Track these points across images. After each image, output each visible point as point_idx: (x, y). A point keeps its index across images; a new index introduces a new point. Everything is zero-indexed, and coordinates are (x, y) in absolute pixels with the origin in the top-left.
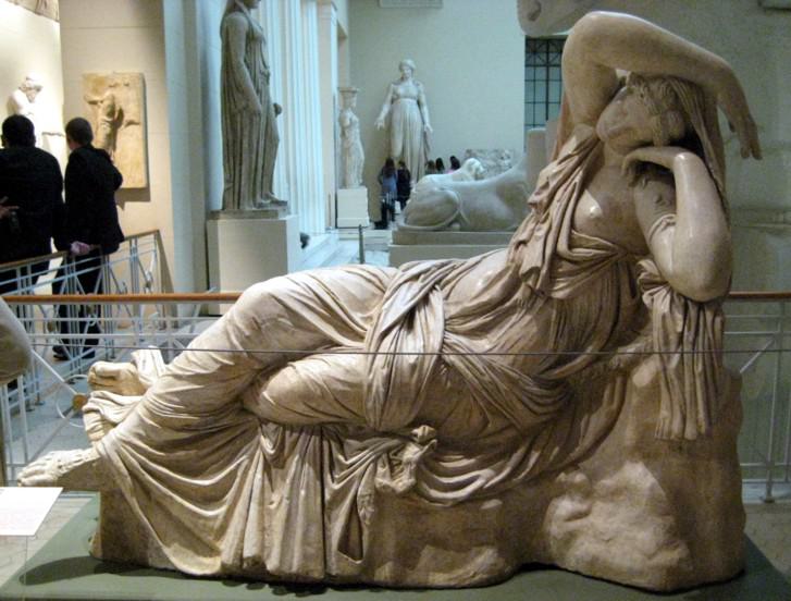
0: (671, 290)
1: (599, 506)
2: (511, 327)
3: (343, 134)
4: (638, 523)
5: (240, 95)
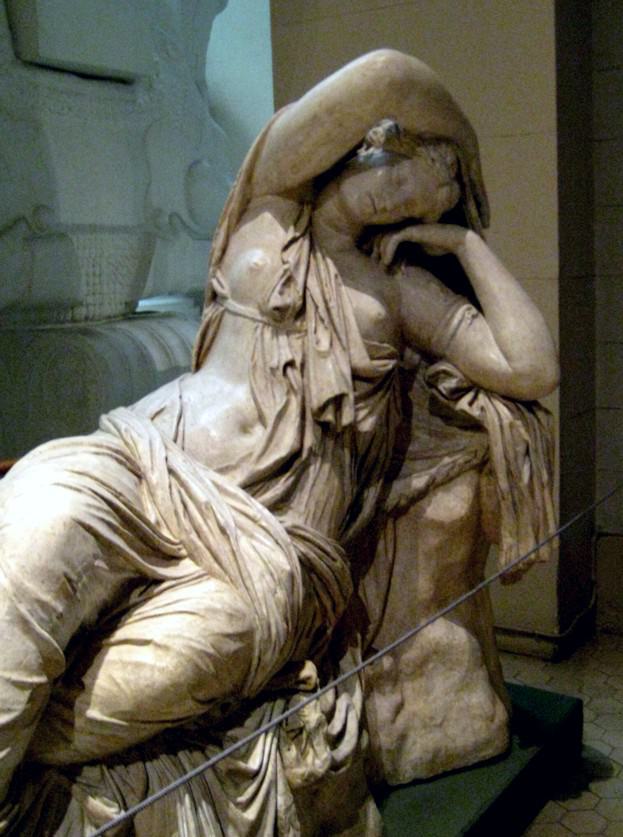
0: (490, 393)
1: (409, 688)
4: (465, 686)
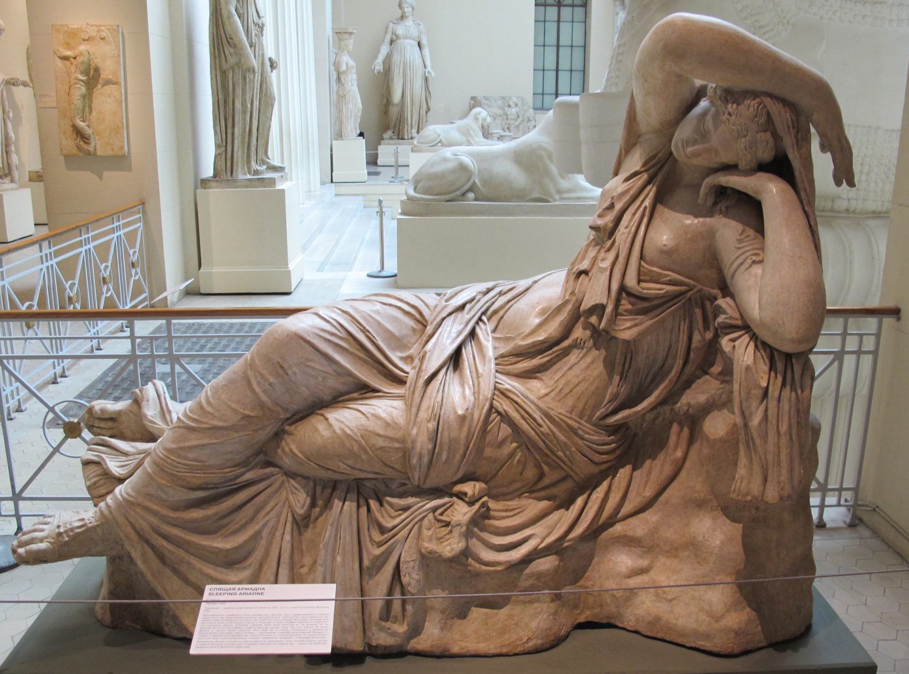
0: (754, 337)
2: (570, 368)
3: (339, 79)
5: (232, 50)
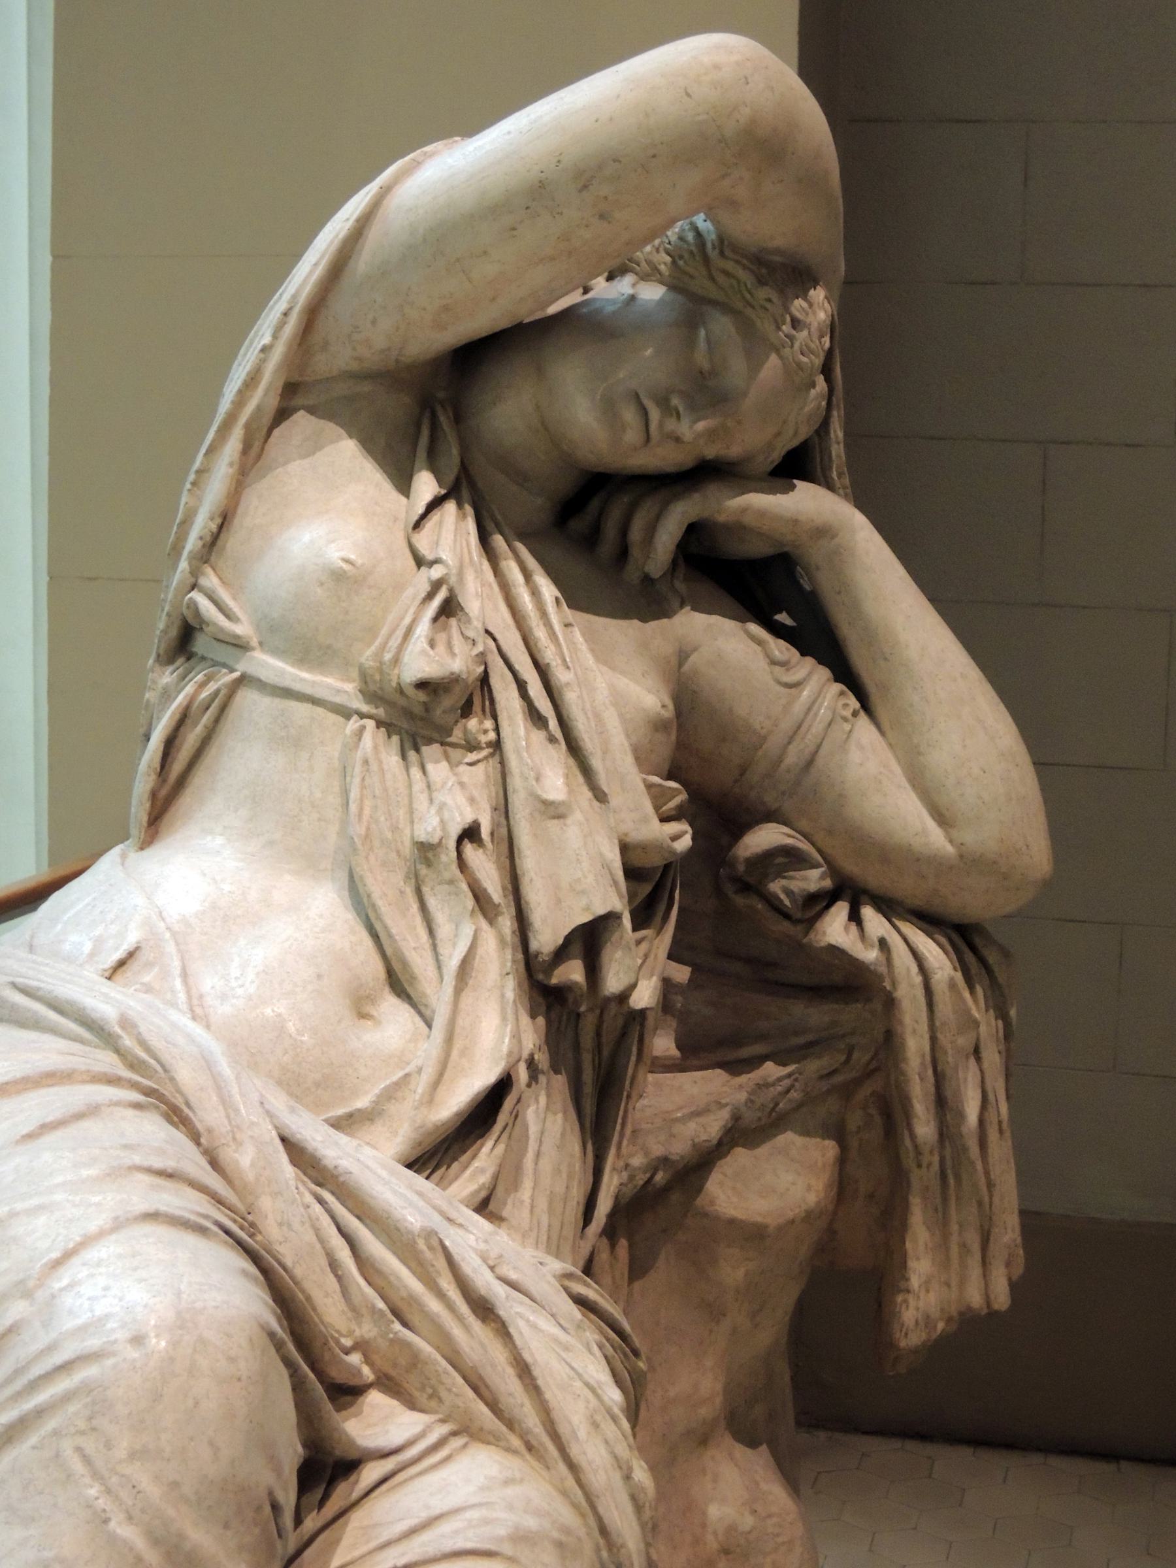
0: (889, 907)
